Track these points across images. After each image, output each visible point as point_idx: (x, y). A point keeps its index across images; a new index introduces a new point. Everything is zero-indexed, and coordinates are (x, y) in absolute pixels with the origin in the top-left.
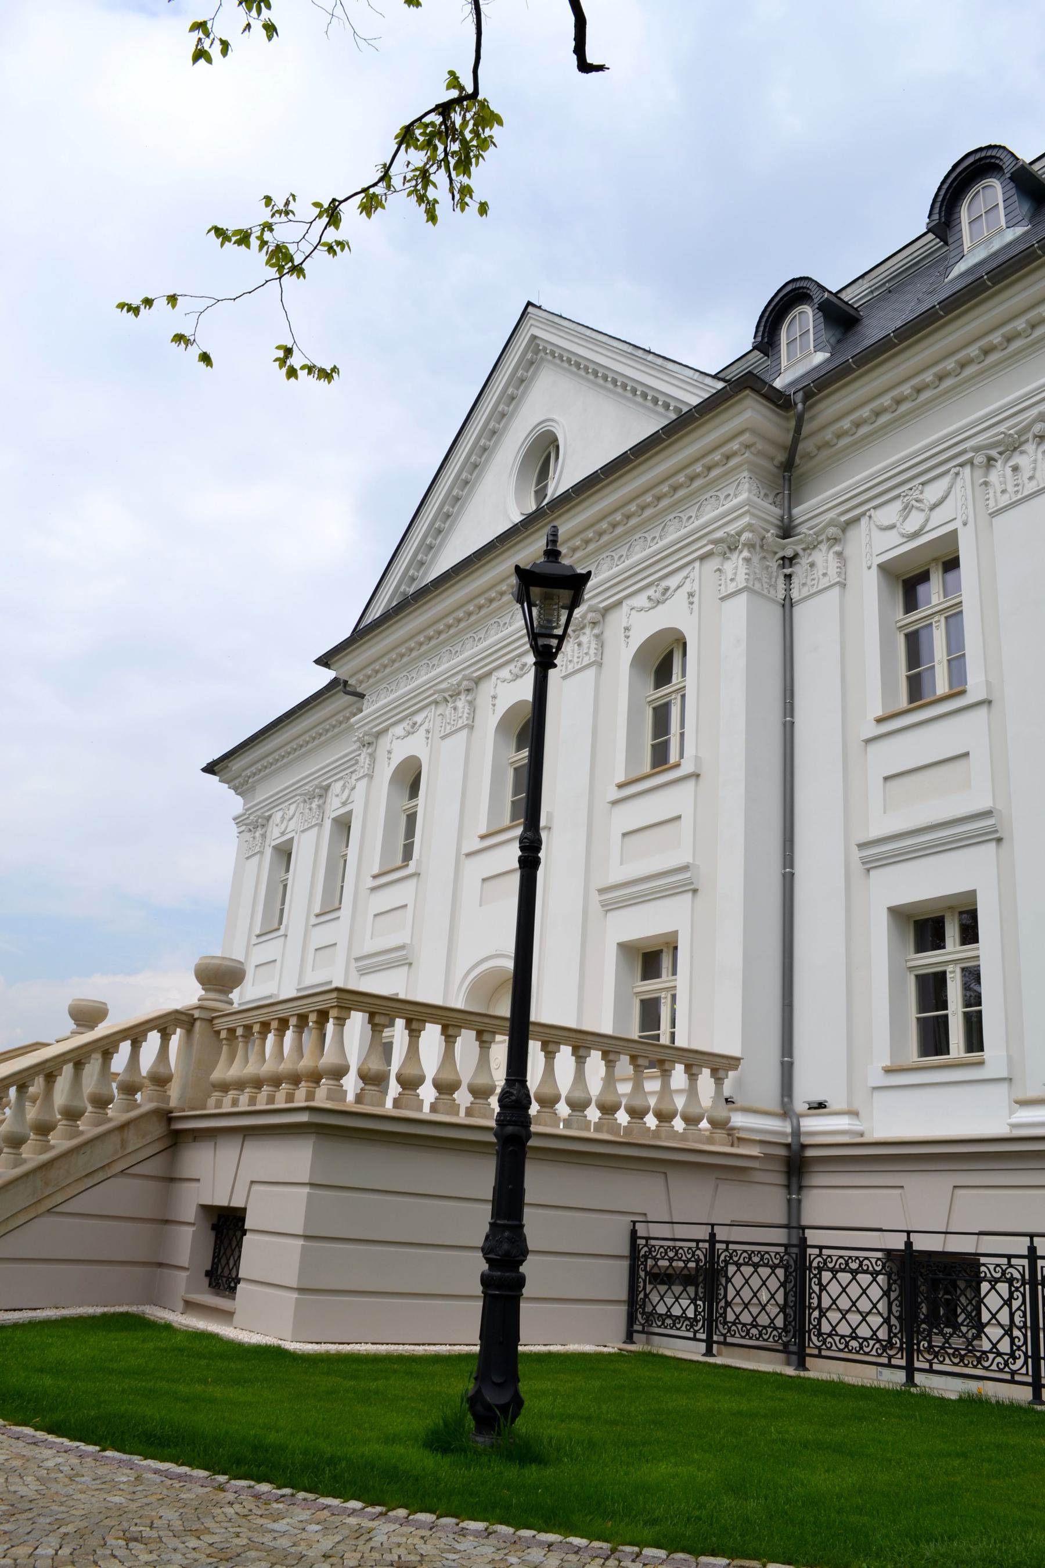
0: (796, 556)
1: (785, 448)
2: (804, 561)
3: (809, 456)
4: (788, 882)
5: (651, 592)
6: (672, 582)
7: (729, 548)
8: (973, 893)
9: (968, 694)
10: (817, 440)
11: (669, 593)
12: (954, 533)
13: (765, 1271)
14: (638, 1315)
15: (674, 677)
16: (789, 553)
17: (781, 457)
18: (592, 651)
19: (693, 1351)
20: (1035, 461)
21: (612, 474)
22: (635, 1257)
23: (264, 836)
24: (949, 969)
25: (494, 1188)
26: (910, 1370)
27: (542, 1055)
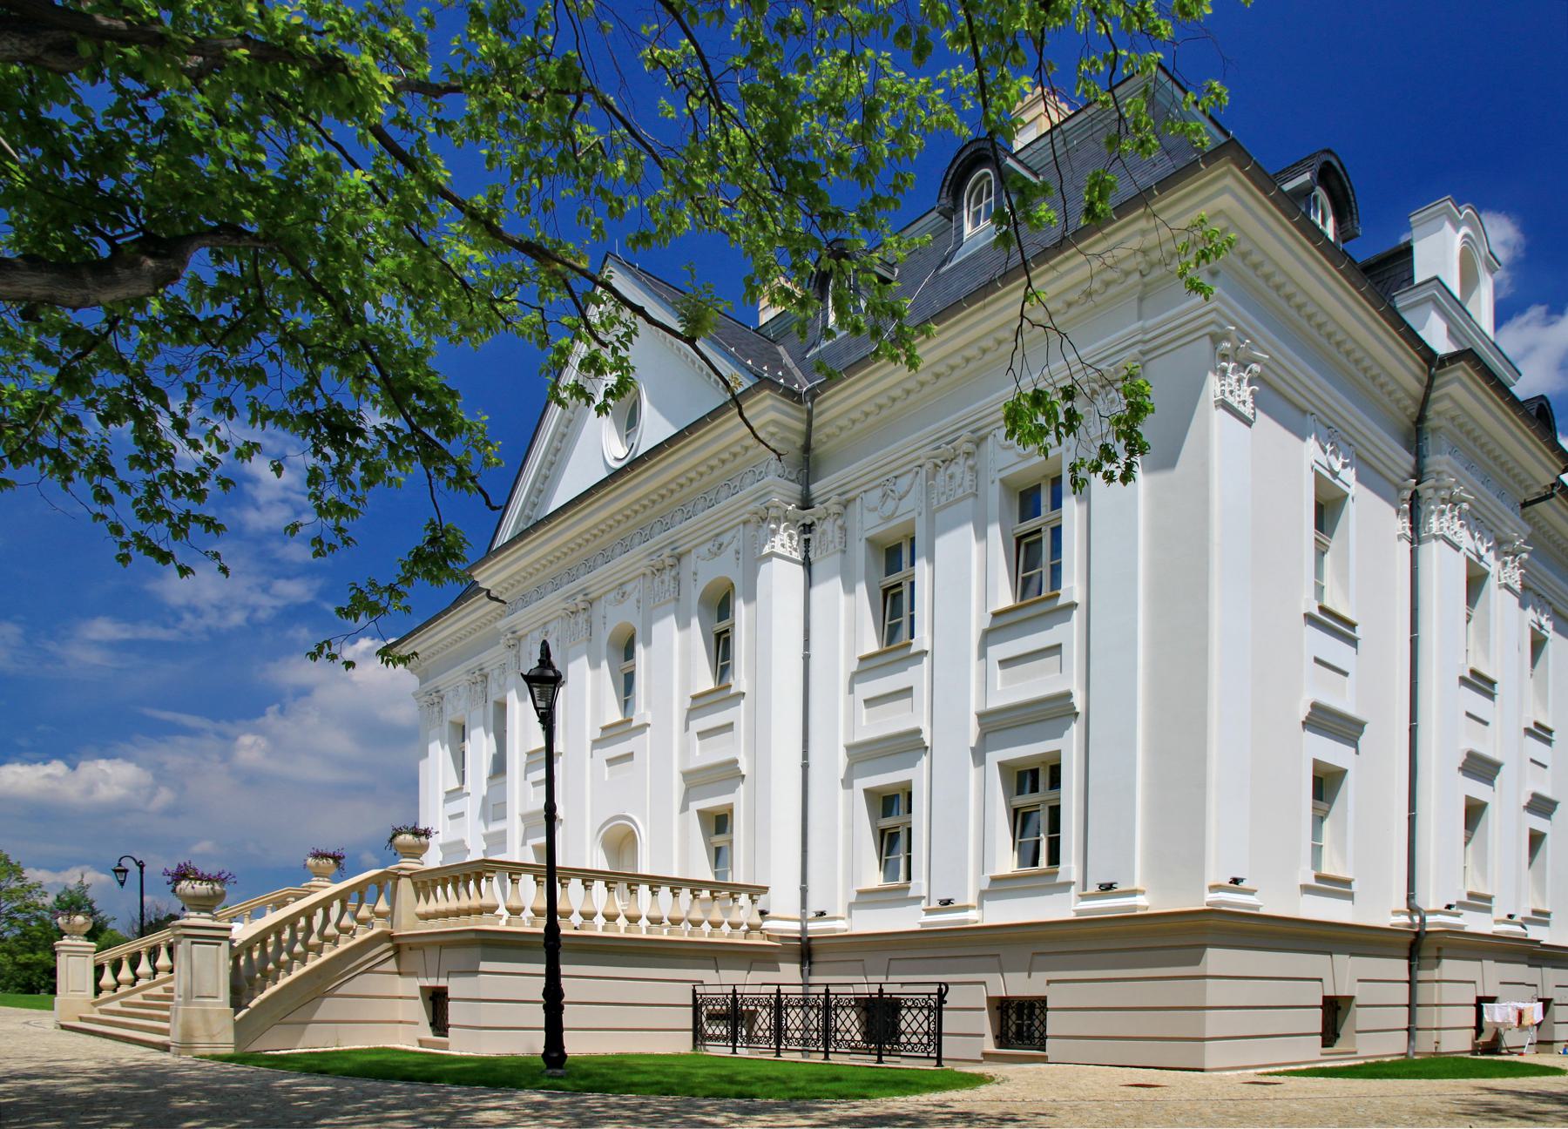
0: (813, 524)
2: (818, 529)
4: (805, 767)
12: (913, 520)
13: (915, 1012)
14: (699, 1036)
15: (1043, 510)
18: (967, 483)
19: (797, 1057)
21: (1128, 213)
22: (696, 1007)
25: (1352, 954)
26: (734, 1048)
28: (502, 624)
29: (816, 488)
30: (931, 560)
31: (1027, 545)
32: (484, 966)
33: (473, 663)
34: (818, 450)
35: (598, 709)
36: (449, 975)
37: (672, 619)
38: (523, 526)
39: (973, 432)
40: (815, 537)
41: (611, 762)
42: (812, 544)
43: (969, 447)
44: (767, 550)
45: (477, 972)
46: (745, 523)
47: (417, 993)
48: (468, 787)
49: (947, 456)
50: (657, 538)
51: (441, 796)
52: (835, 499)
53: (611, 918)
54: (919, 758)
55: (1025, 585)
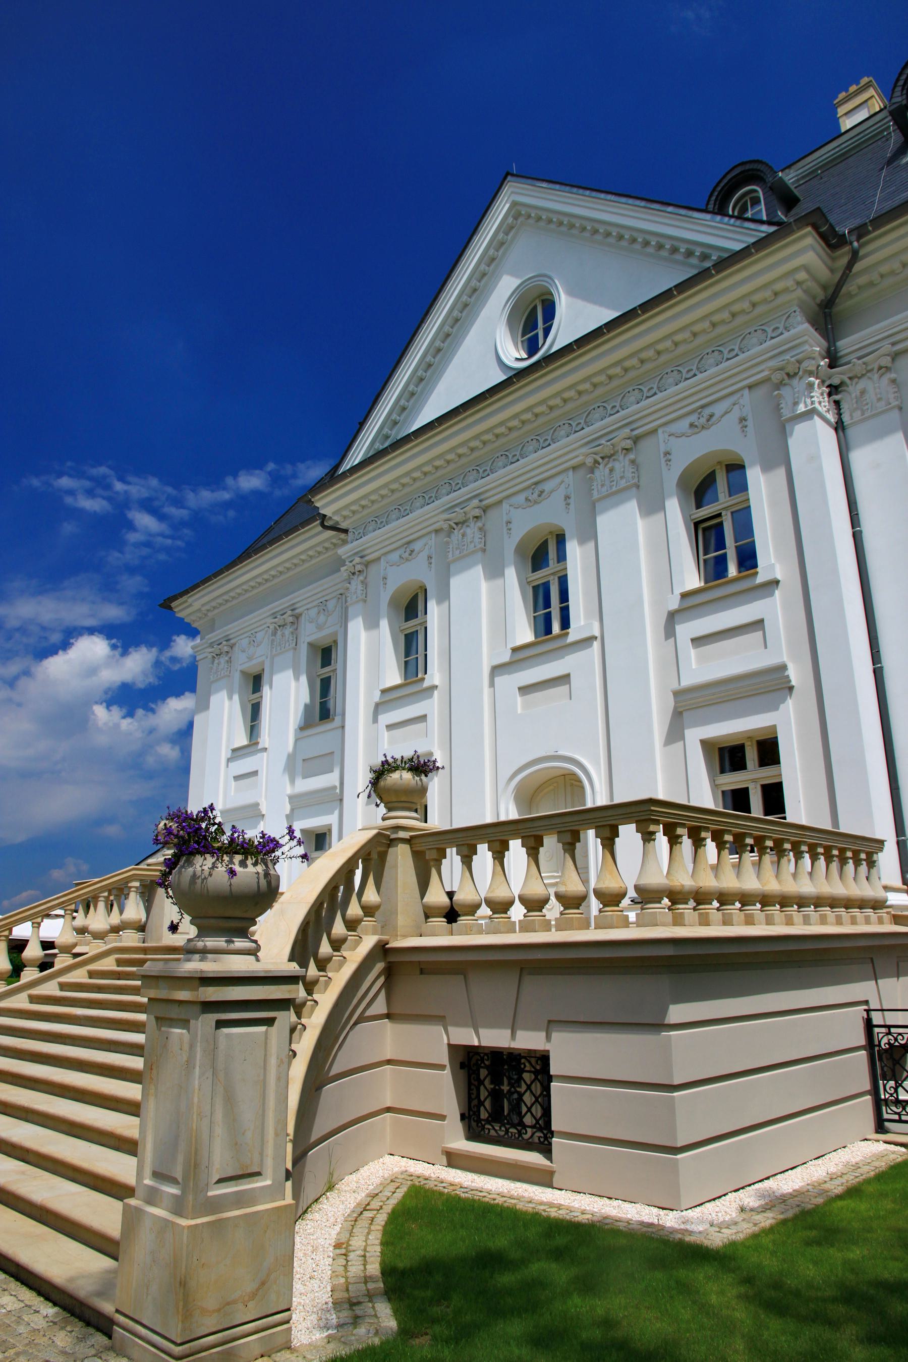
1: (824, 287)
3: (850, 296)
5: (693, 418)
6: (718, 409)
7: (788, 374)
8: (774, 727)
9: (759, 575)
10: (862, 280)
11: (714, 419)
16: (836, 381)
17: (821, 295)
20: (624, 467)
23: (229, 661)
24: (751, 787)
27: (665, 839)
28: (343, 551)
29: (845, 345)
30: (271, 687)
31: (704, 530)
32: (677, 1013)
33: (282, 603)
34: (843, 305)
35: (501, 625)
36: (551, 1025)
37: (478, 570)
38: (379, 446)
39: (893, 344)
40: (848, 401)
41: (525, 690)
42: (845, 406)
43: (628, 443)
44: (801, 408)
45: (660, 1026)
46: (437, 531)
47: (444, 1057)
48: (265, 740)
49: (608, 451)
50: (472, 486)
51: (225, 754)
52: (290, 613)
53: (534, 905)
54: (784, 700)
55: (544, 627)
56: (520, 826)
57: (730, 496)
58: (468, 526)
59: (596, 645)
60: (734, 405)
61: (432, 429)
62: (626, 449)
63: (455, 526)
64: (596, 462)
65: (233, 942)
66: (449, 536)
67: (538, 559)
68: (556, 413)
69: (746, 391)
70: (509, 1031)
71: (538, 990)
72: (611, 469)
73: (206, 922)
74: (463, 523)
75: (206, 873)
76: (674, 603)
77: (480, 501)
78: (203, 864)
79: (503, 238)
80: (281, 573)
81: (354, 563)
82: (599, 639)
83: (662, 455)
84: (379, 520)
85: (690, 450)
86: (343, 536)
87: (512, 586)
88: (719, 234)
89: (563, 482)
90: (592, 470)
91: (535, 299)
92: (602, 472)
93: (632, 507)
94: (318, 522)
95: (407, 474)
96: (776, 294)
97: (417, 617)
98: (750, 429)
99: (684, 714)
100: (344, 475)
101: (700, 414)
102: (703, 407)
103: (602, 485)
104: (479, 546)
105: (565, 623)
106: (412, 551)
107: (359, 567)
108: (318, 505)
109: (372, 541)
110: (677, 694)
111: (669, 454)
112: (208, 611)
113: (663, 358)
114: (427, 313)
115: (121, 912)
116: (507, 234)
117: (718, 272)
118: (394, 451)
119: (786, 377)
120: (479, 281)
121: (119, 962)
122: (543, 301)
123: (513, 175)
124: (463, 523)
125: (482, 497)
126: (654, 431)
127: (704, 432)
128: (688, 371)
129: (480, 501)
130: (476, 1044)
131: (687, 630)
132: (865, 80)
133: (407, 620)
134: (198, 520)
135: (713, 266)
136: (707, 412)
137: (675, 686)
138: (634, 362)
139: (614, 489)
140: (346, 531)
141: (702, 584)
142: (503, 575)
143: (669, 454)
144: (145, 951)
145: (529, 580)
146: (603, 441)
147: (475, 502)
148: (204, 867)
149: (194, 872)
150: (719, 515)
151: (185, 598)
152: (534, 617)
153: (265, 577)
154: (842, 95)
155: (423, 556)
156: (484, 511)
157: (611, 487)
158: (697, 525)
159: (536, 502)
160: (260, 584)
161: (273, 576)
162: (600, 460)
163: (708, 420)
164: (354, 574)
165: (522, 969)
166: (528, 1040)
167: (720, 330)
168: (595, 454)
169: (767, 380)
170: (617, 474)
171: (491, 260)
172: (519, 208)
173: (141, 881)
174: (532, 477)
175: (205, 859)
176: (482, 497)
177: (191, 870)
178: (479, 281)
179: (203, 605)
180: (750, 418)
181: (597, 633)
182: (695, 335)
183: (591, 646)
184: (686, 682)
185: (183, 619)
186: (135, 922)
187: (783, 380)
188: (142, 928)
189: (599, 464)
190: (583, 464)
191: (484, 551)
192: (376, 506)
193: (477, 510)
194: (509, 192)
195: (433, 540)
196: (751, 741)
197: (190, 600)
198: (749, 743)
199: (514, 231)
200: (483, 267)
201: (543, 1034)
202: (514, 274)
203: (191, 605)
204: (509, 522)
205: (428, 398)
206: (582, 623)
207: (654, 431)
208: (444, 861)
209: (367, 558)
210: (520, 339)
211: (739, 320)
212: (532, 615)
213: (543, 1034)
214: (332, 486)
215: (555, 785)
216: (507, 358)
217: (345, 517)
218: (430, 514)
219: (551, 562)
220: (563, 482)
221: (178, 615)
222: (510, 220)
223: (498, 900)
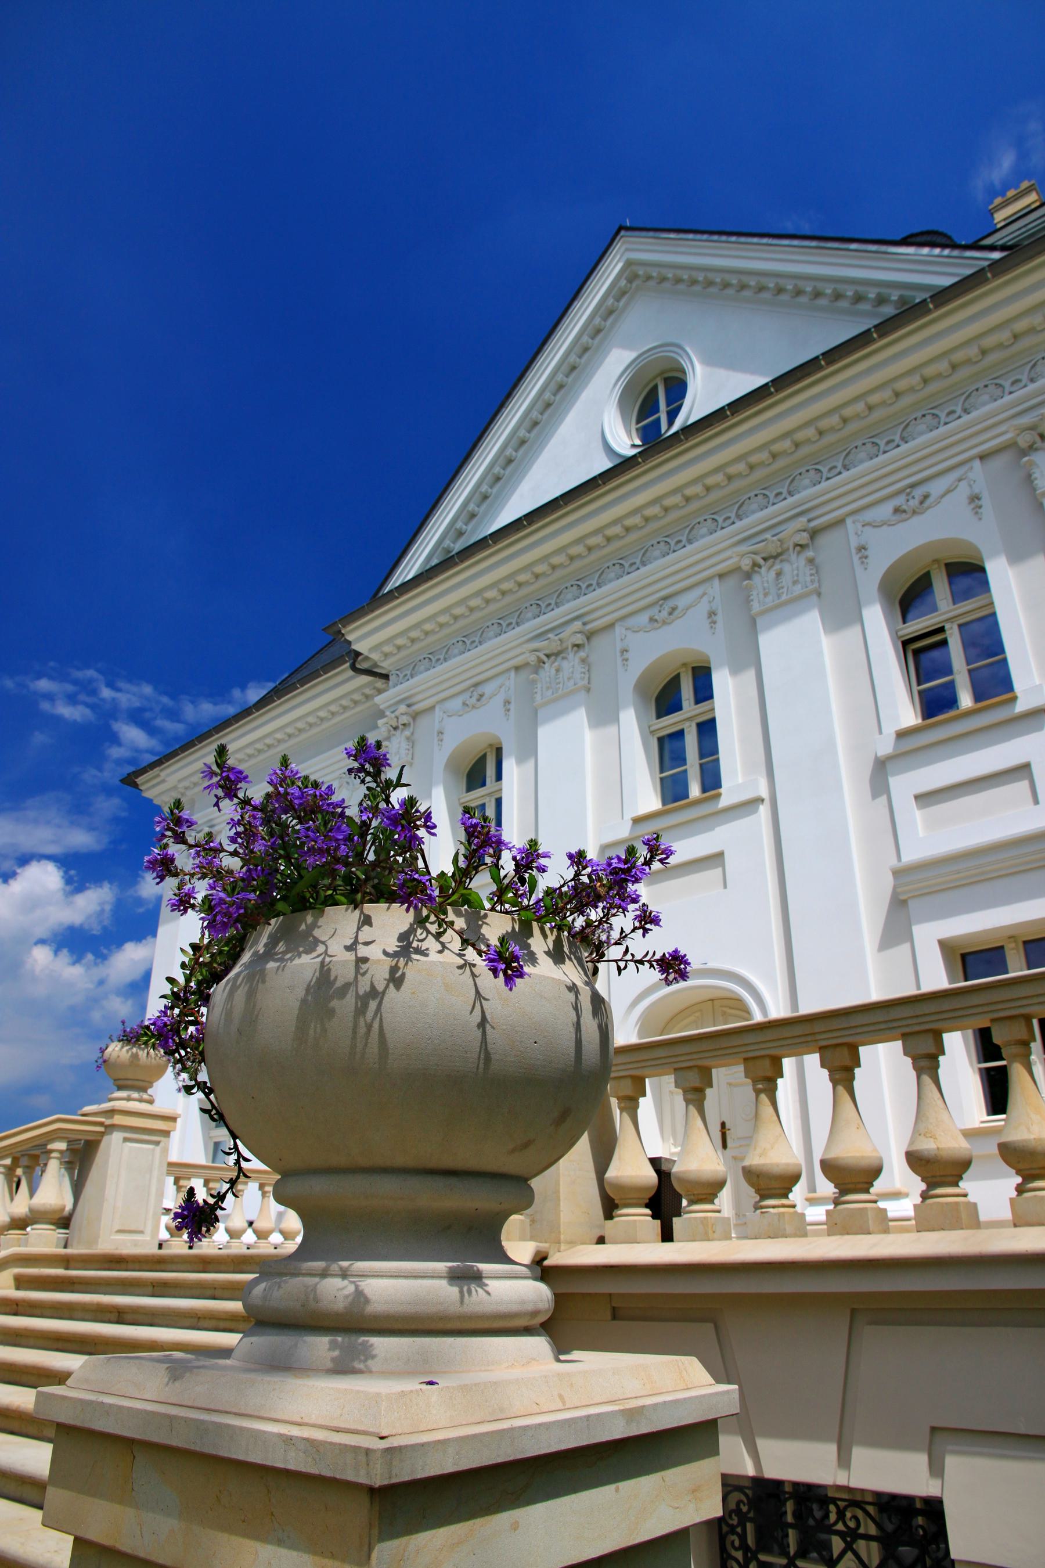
6: (936, 488)
35: (617, 787)
36: (939, 1439)
37: (580, 716)
43: (803, 538)
49: (772, 549)
56: (818, 1027)
57: (954, 604)
58: (564, 658)
59: (764, 810)
60: (960, 480)
61: (518, 530)
62: (801, 546)
63: (545, 659)
64: (755, 565)
65: (477, 1277)
66: (536, 673)
67: (666, 701)
68: (694, 505)
69: (977, 463)
70: (833, 1448)
71: (894, 1358)
72: (783, 566)
73: (317, 1187)
74: (557, 654)
75: (379, 972)
76: (886, 746)
77: (584, 624)
78: (359, 937)
79: (613, 304)
80: (290, 736)
81: (397, 713)
82: (767, 802)
83: (854, 551)
84: (433, 658)
85: (895, 544)
86: (380, 683)
87: (632, 733)
88: (926, 269)
89: (704, 594)
90: (748, 576)
91: (655, 378)
92: (766, 576)
93: (811, 620)
94: (348, 664)
95: (479, 593)
96: (1016, 337)
97: (484, 784)
98: (720, 625)
99: (910, 902)
100: (392, 595)
101: (908, 494)
102: (913, 486)
103: (766, 595)
104: (581, 683)
105: (712, 781)
106: (481, 696)
107: (404, 719)
108: (350, 638)
109: (421, 685)
110: (897, 873)
111: (865, 549)
112: (186, 788)
113: (852, 427)
114: (509, 395)
115: (32, 1193)
116: (618, 300)
117: (937, 307)
118: (462, 561)
119: (1038, 439)
120: (542, 414)
121: (21, 1282)
122: (667, 380)
123: (627, 229)
124: (557, 654)
125: (586, 619)
126: (841, 522)
127: (916, 520)
128: (888, 443)
129: (584, 624)
130: (750, 1471)
131: (906, 784)
132: (1025, 184)
133: (469, 789)
134: (173, 697)
135: (931, 297)
136: (918, 492)
137: (893, 862)
138: (810, 432)
139: (784, 597)
140: (386, 677)
141: (920, 721)
142: (617, 720)
143: (865, 549)
144: (67, 1262)
145: (652, 728)
146: (768, 536)
147: (577, 625)
148: (363, 951)
149: (325, 974)
150: (942, 630)
151: (156, 770)
152: (662, 779)
153: (268, 741)
154: (998, 201)
155: (499, 700)
156: (588, 638)
157: (779, 596)
158: (905, 644)
159: (664, 623)
160: (260, 751)
161: (279, 741)
162: (762, 562)
163: (921, 503)
164: (396, 728)
165: (853, 1312)
166: (889, 1470)
167: (933, 387)
168: (755, 554)
169: (1012, 445)
170: (786, 580)
171: (598, 332)
172: (634, 268)
173: (70, 1142)
174: (657, 592)
175: (367, 921)
176: (586, 619)
177: (306, 964)
178: (542, 414)
179: (180, 781)
180: (720, 612)
181: (764, 792)
182: (897, 395)
183: (756, 811)
184: (911, 855)
185: (151, 801)
186: (54, 1212)
187: (1034, 443)
188: (64, 1222)
189: (760, 567)
190: (737, 569)
191: (588, 690)
192: (431, 639)
193: (579, 635)
194: (623, 249)
195: (512, 681)
196: (1015, 941)
197: (163, 774)
198: (1013, 945)
199: (627, 296)
200: (585, 339)
201: (923, 1458)
202: (625, 346)
203: (163, 781)
204: (624, 651)
205: (509, 499)
206: (740, 781)
207: (841, 522)
208: (641, 1100)
209: (415, 708)
210: (634, 427)
211: (963, 373)
212: (658, 776)
213: (922, 1459)
214: (372, 611)
215: (697, 1014)
216: (619, 445)
217: (386, 655)
218: (513, 644)
219: (685, 704)
220: (704, 594)
221: (147, 794)
222: (623, 283)
223: (776, 1170)
